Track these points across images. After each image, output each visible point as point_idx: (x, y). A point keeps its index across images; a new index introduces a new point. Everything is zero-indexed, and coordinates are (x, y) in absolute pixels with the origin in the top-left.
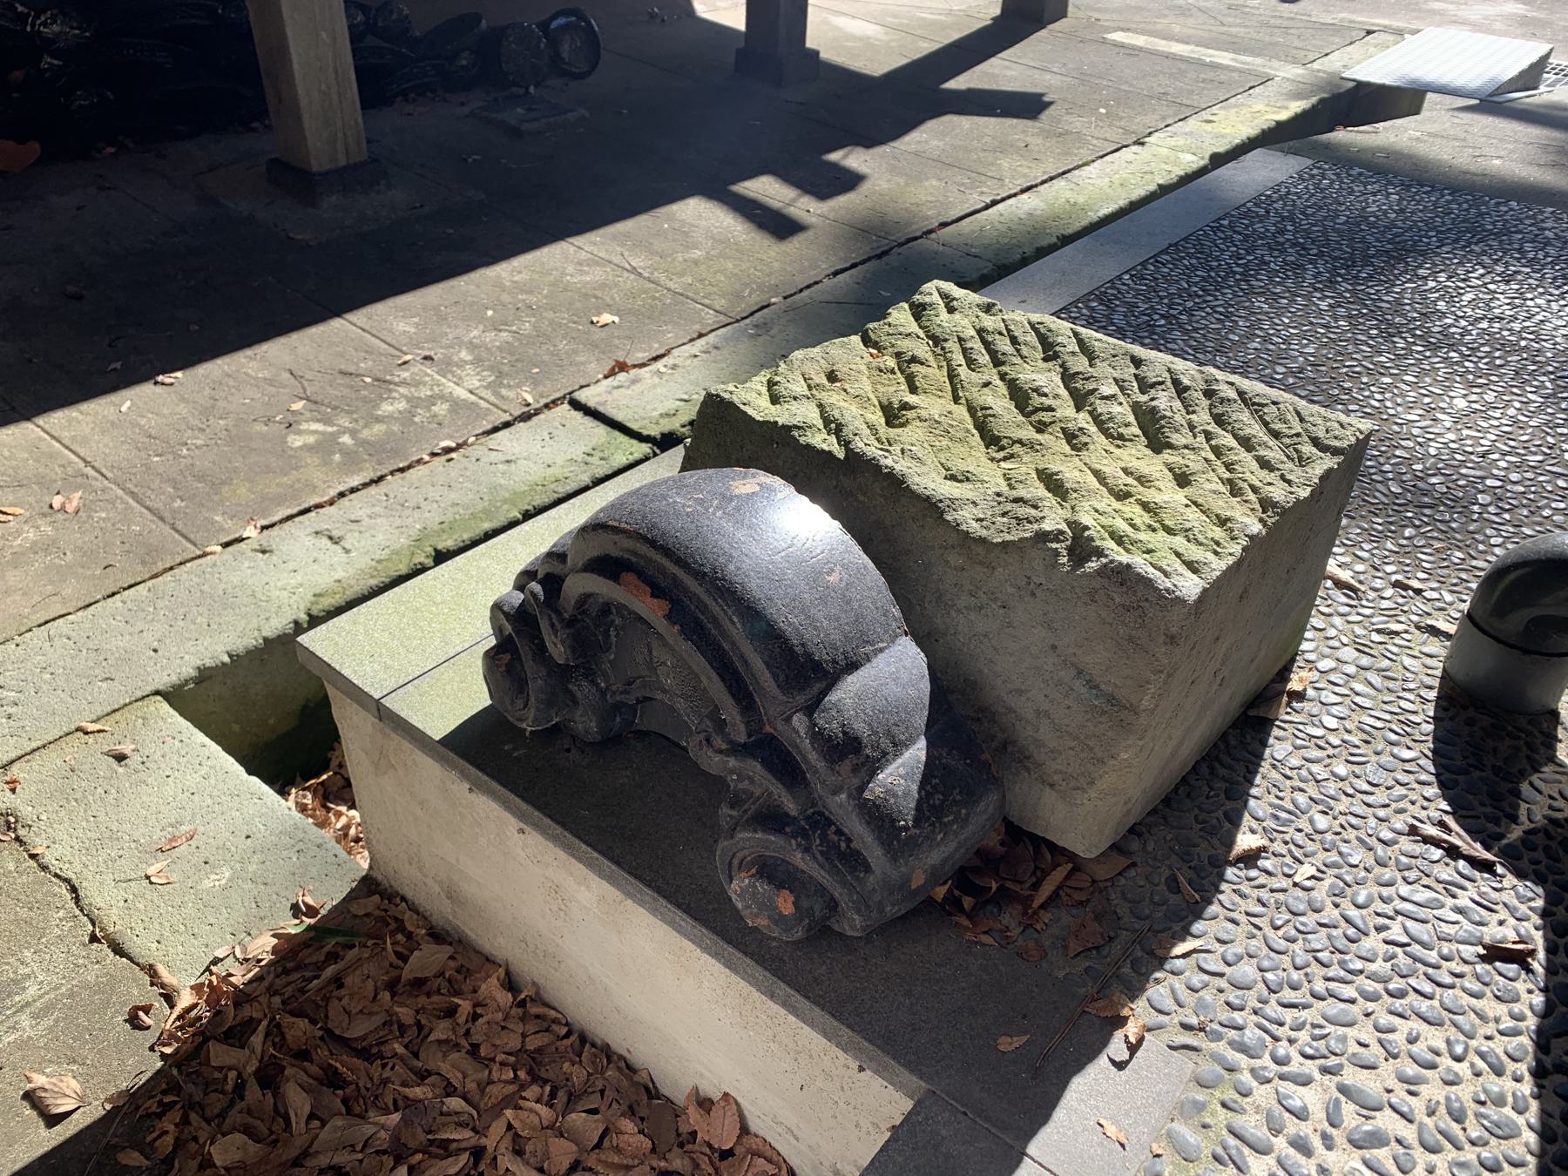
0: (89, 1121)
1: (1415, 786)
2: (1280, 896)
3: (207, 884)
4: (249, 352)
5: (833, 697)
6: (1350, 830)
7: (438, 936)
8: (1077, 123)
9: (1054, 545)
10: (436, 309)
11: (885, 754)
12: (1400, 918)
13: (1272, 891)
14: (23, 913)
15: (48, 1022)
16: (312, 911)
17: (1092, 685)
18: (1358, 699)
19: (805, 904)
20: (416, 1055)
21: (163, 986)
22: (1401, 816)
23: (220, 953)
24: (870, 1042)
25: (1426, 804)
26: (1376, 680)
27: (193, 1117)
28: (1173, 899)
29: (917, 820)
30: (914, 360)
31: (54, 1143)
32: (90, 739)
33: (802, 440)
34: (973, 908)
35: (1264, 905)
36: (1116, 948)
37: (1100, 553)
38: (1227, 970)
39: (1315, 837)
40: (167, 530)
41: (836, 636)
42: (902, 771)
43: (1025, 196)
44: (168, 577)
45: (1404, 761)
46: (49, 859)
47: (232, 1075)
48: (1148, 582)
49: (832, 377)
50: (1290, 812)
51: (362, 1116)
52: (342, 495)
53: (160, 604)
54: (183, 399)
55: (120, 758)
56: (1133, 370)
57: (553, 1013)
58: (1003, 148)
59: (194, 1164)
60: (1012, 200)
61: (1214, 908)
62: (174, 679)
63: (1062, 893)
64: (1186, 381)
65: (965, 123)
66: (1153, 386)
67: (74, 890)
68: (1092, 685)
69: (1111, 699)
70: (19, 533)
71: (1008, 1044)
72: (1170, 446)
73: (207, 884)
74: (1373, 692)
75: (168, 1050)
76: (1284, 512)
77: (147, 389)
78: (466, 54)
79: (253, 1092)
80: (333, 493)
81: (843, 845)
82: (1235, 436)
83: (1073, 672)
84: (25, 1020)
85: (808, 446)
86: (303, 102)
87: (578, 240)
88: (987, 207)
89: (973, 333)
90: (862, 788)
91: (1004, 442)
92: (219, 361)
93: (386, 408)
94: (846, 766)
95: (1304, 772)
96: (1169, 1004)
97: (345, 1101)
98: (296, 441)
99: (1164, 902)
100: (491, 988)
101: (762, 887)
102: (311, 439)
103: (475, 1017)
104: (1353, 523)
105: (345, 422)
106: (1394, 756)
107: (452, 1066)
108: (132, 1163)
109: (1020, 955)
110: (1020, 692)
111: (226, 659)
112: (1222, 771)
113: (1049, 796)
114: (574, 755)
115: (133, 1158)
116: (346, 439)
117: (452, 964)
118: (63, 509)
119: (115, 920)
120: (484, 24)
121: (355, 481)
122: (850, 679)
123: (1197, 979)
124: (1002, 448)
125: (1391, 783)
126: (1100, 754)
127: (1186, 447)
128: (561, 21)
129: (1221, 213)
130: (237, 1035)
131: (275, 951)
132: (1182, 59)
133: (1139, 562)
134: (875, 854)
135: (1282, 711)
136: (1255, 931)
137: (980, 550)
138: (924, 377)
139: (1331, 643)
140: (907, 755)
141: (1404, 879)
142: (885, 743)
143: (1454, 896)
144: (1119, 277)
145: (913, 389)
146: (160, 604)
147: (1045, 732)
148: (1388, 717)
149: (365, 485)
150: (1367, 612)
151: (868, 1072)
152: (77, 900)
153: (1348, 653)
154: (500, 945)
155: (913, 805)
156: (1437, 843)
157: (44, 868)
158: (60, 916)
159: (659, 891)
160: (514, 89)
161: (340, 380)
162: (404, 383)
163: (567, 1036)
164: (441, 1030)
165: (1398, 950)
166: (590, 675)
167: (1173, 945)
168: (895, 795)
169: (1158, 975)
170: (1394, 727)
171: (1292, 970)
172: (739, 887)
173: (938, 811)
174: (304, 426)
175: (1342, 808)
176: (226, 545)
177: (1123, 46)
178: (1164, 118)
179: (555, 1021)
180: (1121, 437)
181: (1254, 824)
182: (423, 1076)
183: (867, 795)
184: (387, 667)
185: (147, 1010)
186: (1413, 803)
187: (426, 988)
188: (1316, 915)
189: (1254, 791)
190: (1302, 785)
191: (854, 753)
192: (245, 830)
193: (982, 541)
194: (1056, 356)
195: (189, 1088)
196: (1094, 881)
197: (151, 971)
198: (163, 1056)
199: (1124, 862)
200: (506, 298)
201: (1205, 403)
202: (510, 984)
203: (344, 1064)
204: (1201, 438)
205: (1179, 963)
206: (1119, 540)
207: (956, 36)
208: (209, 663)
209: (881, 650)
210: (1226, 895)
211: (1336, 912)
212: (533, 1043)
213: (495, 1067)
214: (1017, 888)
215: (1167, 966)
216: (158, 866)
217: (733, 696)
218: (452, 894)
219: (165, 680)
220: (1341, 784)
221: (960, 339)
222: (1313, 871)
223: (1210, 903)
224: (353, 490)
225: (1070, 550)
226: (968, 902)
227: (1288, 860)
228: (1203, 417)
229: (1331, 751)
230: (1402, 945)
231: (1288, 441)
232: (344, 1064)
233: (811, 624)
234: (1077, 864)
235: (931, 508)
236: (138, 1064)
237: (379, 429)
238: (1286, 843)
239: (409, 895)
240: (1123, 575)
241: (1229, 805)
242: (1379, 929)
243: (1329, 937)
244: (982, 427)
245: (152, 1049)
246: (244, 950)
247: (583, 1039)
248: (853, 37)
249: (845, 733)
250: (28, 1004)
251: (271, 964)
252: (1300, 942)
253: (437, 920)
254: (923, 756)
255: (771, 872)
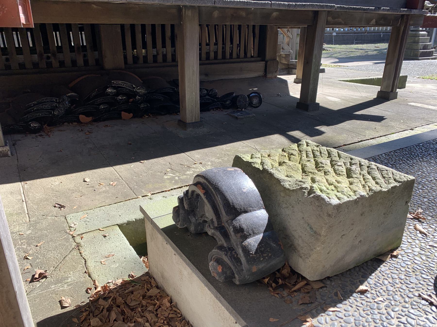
0: (70, 310)
1: (426, 285)
2: (369, 304)
3: (113, 266)
4: (162, 158)
5: (239, 218)
6: (399, 292)
7: (157, 287)
8: (393, 124)
9: (304, 191)
10: (206, 153)
11: (250, 235)
12: (406, 317)
13: (367, 302)
14: (74, 264)
15: (70, 287)
16: (132, 277)
17: (311, 228)
18: (416, 261)
19: (225, 270)
20: (143, 313)
21: (96, 285)
22: (418, 292)
23: (110, 281)
24: (235, 311)
25: (427, 290)
26: (424, 258)
27: (91, 314)
28: (335, 298)
29: (255, 253)
30: (292, 154)
31: (61, 313)
32: (100, 232)
33: (253, 166)
34: (275, 288)
35: (362, 305)
36: (313, 305)
37: (314, 193)
38: (344, 318)
39: (387, 292)
40: (132, 192)
41: (242, 203)
42: (254, 240)
43: (371, 140)
44: (128, 201)
45: (424, 278)
46: (83, 254)
47: (102, 307)
48: (323, 199)
49: (269, 156)
50: (380, 284)
51: (126, 323)
52: (172, 189)
53: (125, 206)
54: (145, 166)
55: (105, 236)
56: (350, 161)
57: (178, 311)
58: (367, 129)
59: (87, 325)
60: (367, 141)
61: (347, 302)
62: (122, 222)
63: (302, 289)
64: (362, 164)
65: (358, 122)
66: (353, 164)
67: (86, 262)
68: (311, 228)
69: (315, 232)
70: (102, 188)
71: (271, 320)
72: (352, 177)
73: (113, 266)
74: (421, 260)
75: (91, 299)
76: (375, 192)
77: (138, 163)
78: (229, 101)
79: (105, 311)
80: (170, 189)
81: (235, 256)
82: (372, 177)
83: (307, 225)
84: (66, 286)
85: (255, 167)
86: (187, 107)
87: (244, 142)
88: (359, 142)
89: (311, 150)
90: (242, 242)
91: (307, 172)
92: (155, 159)
93: (188, 172)
94: (239, 235)
95: (389, 276)
96: (323, 322)
97: (124, 319)
98: (166, 177)
99: (332, 298)
100: (166, 301)
101: (215, 264)
102: (169, 177)
103: (160, 307)
104: (433, 219)
105: (178, 174)
106: (421, 277)
107: (149, 316)
108: (75, 321)
109: (285, 301)
110: (296, 231)
111: (134, 220)
112: (363, 270)
113: (300, 260)
114: (190, 237)
115: (75, 320)
116: (177, 178)
117: (159, 294)
118: (112, 185)
119: (91, 269)
120: (234, 95)
121: (176, 187)
122: (244, 215)
123: (334, 317)
124: (306, 173)
125: (418, 283)
126: (312, 248)
127: (356, 178)
128: (253, 94)
129: (421, 142)
130: (105, 299)
131: (121, 283)
132: (432, 110)
133: (324, 196)
134: (243, 259)
135: (388, 259)
136: (357, 310)
137: (288, 192)
138: (293, 158)
139: (412, 246)
140: (256, 237)
141: (412, 307)
142: (251, 232)
143: (427, 315)
144: (381, 155)
145: (290, 160)
146: (125, 206)
147: (300, 242)
148: (424, 267)
149: (178, 188)
150: (428, 241)
151: (238, 324)
152: (85, 264)
153: (418, 250)
154: (170, 291)
155: (255, 249)
156: (426, 300)
157: (81, 256)
158: (81, 267)
159: (197, 268)
160: (239, 109)
161: (180, 166)
162: (194, 168)
163: (180, 317)
164: (150, 308)
165: (402, 325)
166: (194, 215)
167: (330, 308)
168: (251, 245)
169: (323, 314)
170: (424, 270)
171: (365, 322)
172: (212, 264)
173: (262, 252)
174: (169, 174)
175: (398, 286)
176: (143, 196)
177: (413, 106)
178: (422, 124)
179: (179, 313)
180: (339, 174)
181: (368, 285)
182: (142, 317)
183: (243, 244)
184: (157, 213)
185: (90, 289)
186: (423, 289)
187: (151, 299)
188: (379, 311)
189: (371, 277)
190: (387, 278)
191: (242, 233)
192: (125, 256)
193: (288, 189)
194: (330, 157)
195: (92, 307)
196: (312, 288)
197: (94, 281)
198: (90, 300)
199: (322, 285)
200: (223, 152)
201: (367, 169)
202: (171, 301)
203: (126, 310)
204: (362, 176)
205: (331, 313)
206: (321, 191)
207: (361, 102)
208: (130, 220)
209: (255, 210)
210: (352, 299)
211: (385, 311)
212: (171, 316)
213: (160, 319)
214: (289, 285)
215: (326, 313)
216: (104, 260)
217: (215, 214)
218: (163, 277)
219: (120, 222)
220: (400, 281)
221: (306, 151)
222: (382, 299)
223: (346, 300)
224: (175, 189)
225: (308, 192)
226: (274, 285)
227: (375, 295)
228: (365, 172)
229: (400, 272)
230: (404, 323)
231: (387, 179)
232: (126, 310)
233: (237, 200)
234: (308, 283)
235: (278, 181)
236: (84, 299)
237: (185, 176)
238: (376, 291)
239: (155, 277)
240: (318, 198)
241: (362, 279)
242: (397, 318)
243: (380, 317)
244: (303, 169)
245: (88, 298)
246: (115, 282)
247: (184, 319)
248: (332, 101)
249: (240, 227)
250: (68, 283)
251: (119, 286)
252: (370, 316)
253: (159, 285)
254: (261, 238)
255: (219, 261)
